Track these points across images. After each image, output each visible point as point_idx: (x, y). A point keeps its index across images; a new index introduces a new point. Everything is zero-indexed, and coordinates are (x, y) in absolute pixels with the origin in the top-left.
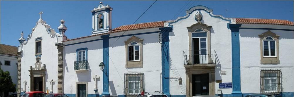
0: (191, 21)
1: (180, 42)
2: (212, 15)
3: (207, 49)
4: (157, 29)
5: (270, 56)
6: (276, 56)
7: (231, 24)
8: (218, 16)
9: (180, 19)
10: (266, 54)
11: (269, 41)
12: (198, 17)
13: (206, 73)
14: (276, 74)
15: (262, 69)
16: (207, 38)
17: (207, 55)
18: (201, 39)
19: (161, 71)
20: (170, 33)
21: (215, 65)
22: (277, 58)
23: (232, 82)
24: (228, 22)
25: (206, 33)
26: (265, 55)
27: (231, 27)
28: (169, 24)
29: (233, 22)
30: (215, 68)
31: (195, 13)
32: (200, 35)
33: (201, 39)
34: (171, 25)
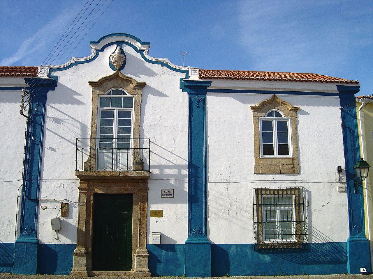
0: (102, 68)
1: (71, 119)
2: (147, 57)
3: (132, 137)
4: (21, 82)
5: (276, 154)
6: (291, 155)
7: (188, 79)
8: (160, 59)
9: (76, 63)
10: (268, 150)
11: (274, 119)
12: (115, 62)
13: (126, 192)
14: (291, 197)
15: (260, 185)
16: (133, 110)
17: (131, 151)
18: (120, 112)
19: (20, 184)
20: (50, 94)
21: (148, 174)
22: (293, 159)
23: (151, 218)
24: (183, 76)
25: (132, 98)
26: (265, 153)
27: (187, 86)
28: (50, 73)
29: (194, 77)
30: (148, 181)
31: (112, 51)
32: (117, 103)
33: (120, 112)
34: (54, 74)
